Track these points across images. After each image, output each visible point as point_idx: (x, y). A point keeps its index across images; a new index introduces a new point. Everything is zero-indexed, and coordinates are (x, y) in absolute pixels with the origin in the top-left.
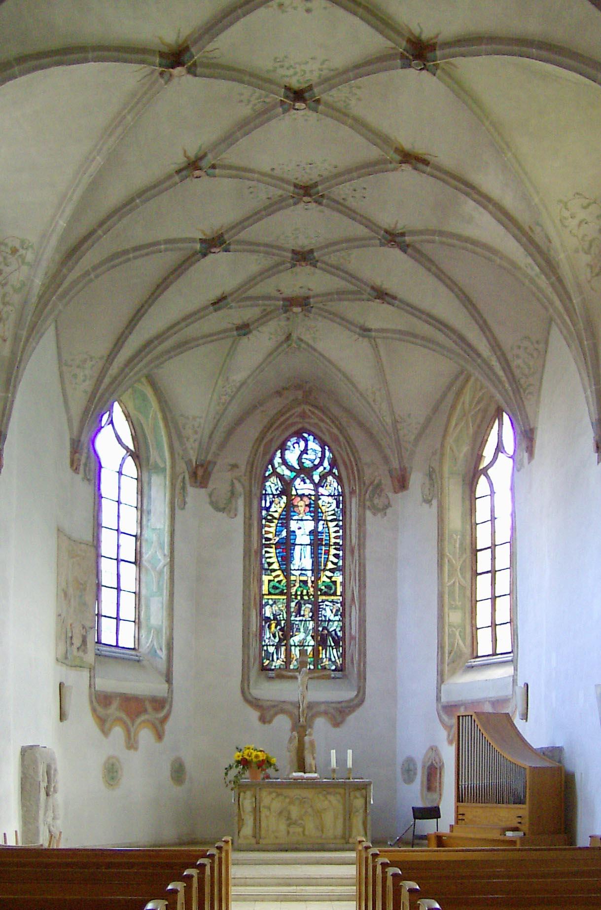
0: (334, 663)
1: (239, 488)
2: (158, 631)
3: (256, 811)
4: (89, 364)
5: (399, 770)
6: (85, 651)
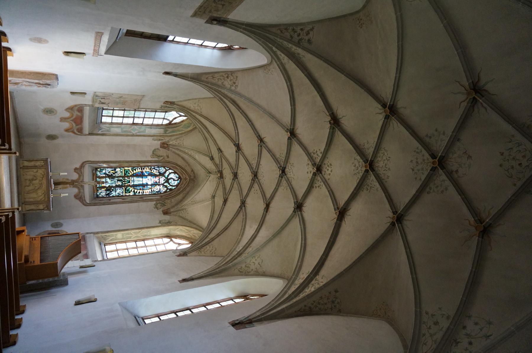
0: (100, 194)
1: (161, 158)
2: (108, 131)
3: (35, 167)
4: (199, 108)
5: (58, 221)
6: (99, 103)
